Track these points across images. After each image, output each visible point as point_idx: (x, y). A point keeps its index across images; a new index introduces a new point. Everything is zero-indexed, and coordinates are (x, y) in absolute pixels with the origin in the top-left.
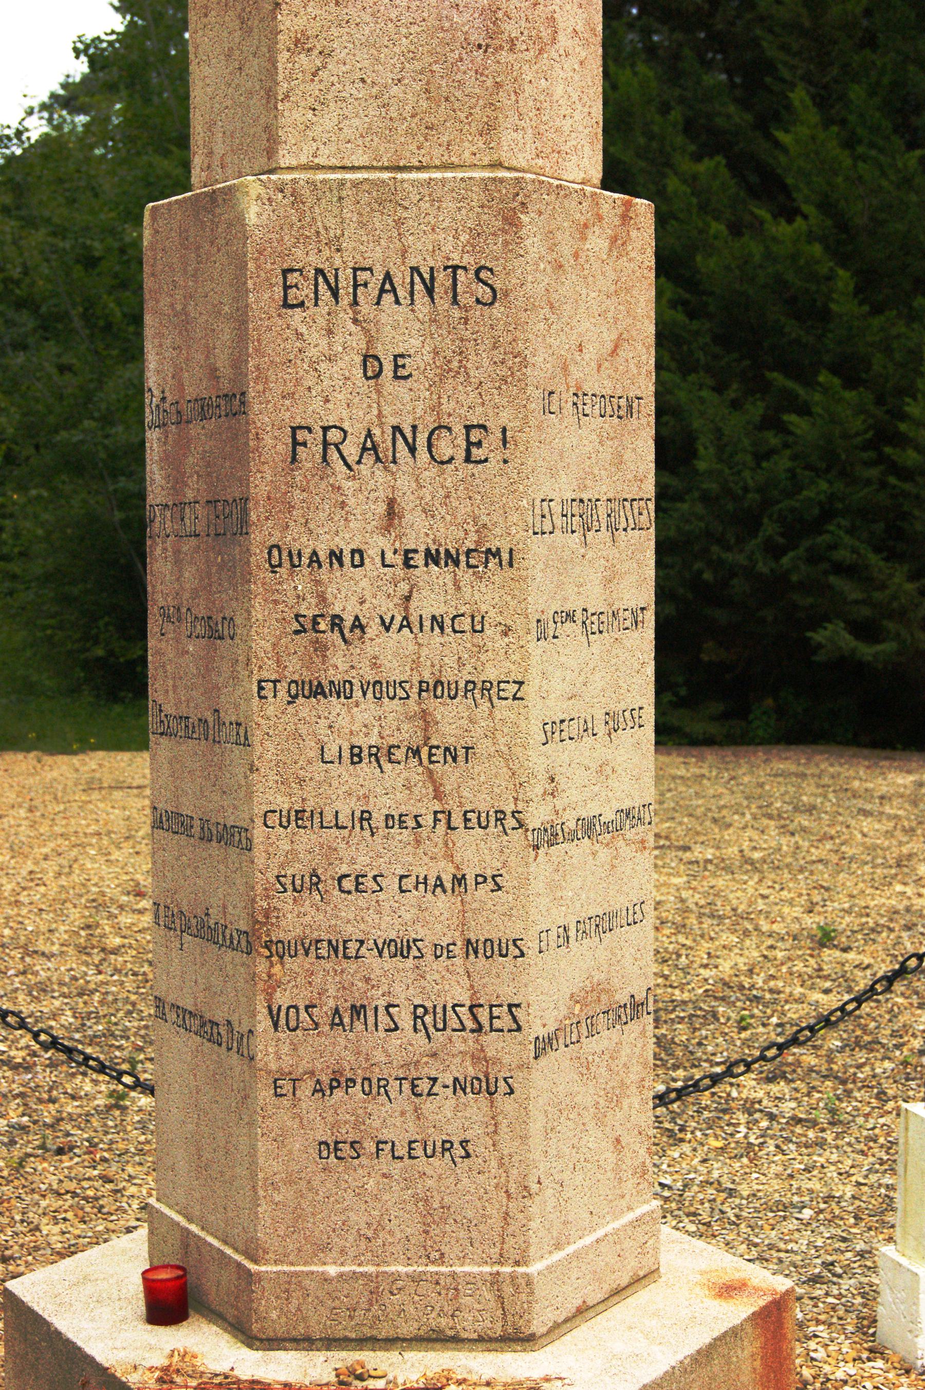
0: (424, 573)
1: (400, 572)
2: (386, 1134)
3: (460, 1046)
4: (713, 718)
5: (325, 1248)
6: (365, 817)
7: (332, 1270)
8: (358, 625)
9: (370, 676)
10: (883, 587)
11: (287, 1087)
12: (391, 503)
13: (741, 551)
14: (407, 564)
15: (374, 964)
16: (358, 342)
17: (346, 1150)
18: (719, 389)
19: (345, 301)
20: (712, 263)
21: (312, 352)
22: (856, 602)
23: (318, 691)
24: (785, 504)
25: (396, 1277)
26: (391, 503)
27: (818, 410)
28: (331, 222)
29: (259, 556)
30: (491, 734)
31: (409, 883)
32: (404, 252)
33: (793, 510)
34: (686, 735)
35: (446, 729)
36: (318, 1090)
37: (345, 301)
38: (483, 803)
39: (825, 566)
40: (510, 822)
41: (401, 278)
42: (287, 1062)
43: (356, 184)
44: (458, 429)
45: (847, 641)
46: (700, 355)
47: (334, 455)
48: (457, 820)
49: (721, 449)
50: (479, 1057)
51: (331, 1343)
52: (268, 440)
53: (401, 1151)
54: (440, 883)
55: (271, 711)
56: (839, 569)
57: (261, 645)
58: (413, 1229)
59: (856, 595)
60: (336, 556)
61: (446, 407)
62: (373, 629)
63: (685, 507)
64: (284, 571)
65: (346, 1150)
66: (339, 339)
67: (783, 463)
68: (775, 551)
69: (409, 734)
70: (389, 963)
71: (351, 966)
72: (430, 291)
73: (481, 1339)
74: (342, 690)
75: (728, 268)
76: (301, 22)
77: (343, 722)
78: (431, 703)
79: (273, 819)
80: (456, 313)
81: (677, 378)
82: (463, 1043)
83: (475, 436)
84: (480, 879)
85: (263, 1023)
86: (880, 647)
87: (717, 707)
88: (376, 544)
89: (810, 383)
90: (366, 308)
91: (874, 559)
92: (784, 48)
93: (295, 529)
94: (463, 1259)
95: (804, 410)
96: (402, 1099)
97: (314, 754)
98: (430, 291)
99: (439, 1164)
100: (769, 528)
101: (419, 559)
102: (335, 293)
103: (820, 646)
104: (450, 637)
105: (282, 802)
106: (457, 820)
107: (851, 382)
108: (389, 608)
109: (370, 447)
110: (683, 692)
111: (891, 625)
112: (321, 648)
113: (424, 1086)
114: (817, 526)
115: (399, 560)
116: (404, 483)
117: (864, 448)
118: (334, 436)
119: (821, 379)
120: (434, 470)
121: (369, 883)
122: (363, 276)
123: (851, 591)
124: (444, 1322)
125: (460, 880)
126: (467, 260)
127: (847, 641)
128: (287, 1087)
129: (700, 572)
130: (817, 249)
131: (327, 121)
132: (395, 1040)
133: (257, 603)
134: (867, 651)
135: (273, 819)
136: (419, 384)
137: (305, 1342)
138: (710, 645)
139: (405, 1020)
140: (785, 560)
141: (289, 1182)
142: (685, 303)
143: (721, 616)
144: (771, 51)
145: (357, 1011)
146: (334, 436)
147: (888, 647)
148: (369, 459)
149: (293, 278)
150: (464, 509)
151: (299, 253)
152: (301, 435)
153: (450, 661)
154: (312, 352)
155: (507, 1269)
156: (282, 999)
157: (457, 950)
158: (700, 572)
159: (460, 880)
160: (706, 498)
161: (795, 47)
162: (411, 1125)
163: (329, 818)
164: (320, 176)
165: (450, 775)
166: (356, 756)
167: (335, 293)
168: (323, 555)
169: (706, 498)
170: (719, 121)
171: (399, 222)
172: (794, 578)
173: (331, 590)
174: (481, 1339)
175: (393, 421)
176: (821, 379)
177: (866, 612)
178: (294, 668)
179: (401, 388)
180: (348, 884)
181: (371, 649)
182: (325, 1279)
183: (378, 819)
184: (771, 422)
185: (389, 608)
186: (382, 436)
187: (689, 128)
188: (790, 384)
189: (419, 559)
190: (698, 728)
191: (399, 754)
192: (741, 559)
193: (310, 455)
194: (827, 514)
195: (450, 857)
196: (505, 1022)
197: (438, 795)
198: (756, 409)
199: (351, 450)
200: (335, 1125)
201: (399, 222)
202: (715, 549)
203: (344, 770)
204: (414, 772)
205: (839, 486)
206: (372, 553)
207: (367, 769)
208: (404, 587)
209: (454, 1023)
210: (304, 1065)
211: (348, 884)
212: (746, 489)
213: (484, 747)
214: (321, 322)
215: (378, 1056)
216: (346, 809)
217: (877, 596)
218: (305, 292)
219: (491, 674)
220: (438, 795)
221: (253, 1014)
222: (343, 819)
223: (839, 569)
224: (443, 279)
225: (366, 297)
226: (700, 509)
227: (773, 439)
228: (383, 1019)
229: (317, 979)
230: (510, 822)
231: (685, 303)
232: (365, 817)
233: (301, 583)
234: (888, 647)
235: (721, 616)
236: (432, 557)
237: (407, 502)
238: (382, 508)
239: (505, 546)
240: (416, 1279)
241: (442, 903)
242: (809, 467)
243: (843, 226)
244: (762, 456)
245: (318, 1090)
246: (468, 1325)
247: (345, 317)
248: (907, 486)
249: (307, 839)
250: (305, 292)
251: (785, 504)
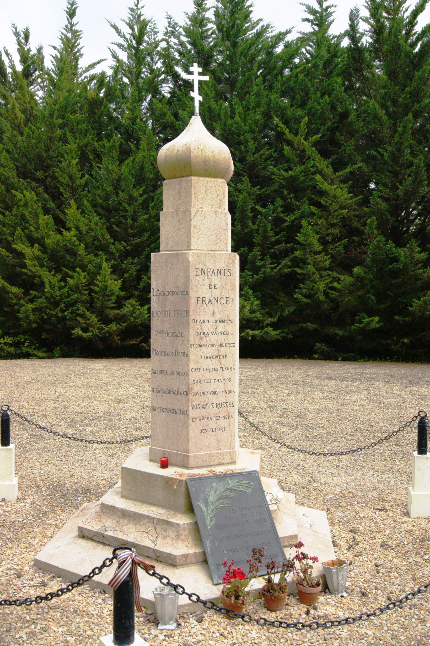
0: (219, 324)
1: (215, 324)
2: (211, 427)
3: (224, 410)
4: (44, 352)
5: (201, 449)
6: (209, 369)
7: (202, 453)
8: (208, 334)
9: (210, 343)
10: (89, 319)
11: (195, 420)
12: (214, 311)
13: (54, 311)
14: (216, 323)
15: (210, 396)
16: (208, 282)
17: (205, 431)
18: (50, 271)
19: (206, 274)
20: (50, 241)
21: (200, 284)
22: (83, 323)
23: (201, 346)
24: (66, 300)
25: (214, 453)
26: (214, 311)
27: (75, 277)
28: (204, 260)
29: (191, 321)
30: (229, 353)
31: (216, 381)
32: (216, 266)
33: (68, 301)
34: (38, 356)
35: (222, 352)
36: (200, 420)
37: (206, 274)
38: (228, 366)
39: (75, 315)
40: (233, 369)
41: (216, 271)
42: (195, 415)
43: (208, 254)
44: (225, 298)
45: (80, 333)
46: (45, 263)
47: (204, 302)
48: (224, 369)
49: (50, 286)
50: (227, 412)
51: (208, 466)
52: (193, 300)
53: (214, 430)
54: (221, 381)
55: (193, 350)
56: (78, 315)
57: (191, 338)
58: (216, 444)
59: (83, 322)
60: (204, 321)
61: (223, 294)
62: (210, 334)
63: (41, 300)
64: (195, 324)
65: (205, 431)
66: (205, 281)
67: (66, 290)
68: (62, 311)
69: (216, 353)
70: (212, 396)
71: (206, 396)
72: (220, 273)
73: (227, 463)
74: (205, 346)
75: (53, 242)
76: (195, 223)
77: (205, 352)
78: (220, 348)
79: (193, 370)
80: (225, 277)
81: (40, 268)
82: (224, 409)
83: (227, 299)
84: (228, 379)
85: (191, 408)
86: (88, 334)
87: (45, 349)
88: (211, 319)
89: (75, 271)
90: (210, 276)
91: (88, 313)
92: (64, 189)
93: (197, 316)
94: (224, 449)
95: (71, 277)
96: (214, 420)
97: (200, 357)
98: (220, 273)
99: (220, 432)
100: (62, 305)
101: (218, 321)
102: (204, 273)
103: (74, 334)
104: (223, 336)
105: (194, 367)
106: (224, 369)
107: (84, 271)
108: (213, 330)
109: (210, 301)
110: (37, 345)
111: (91, 329)
112: (201, 338)
113: (218, 418)
114: (73, 305)
115: (215, 322)
116: (216, 308)
117: (85, 286)
118: (204, 299)
119: (77, 270)
120: (221, 305)
121: (209, 381)
122: (209, 270)
123: (81, 321)
124: (221, 461)
125: (224, 380)
126: (226, 268)
127: (80, 333)
128: (195, 420)
129: (43, 316)
130: (75, 239)
131: (199, 241)
132: (213, 410)
133: (190, 330)
134: (85, 335)
135: (193, 370)
136: (218, 290)
137: (203, 467)
138: (44, 334)
139: (215, 405)
140: (66, 313)
141: (195, 438)
142: (40, 250)
143: (48, 327)
144: (62, 190)
145: (207, 405)
146: (204, 299)
147: (90, 334)
148: (210, 303)
149: (197, 270)
150: (225, 313)
151: (198, 266)
152: (199, 299)
153: (223, 340)
154: (200, 284)
155: (232, 450)
156: (194, 404)
157: (224, 393)
158: (43, 316)
159: (224, 380)
160: (46, 298)
161: (67, 190)
162: (216, 425)
163: (202, 369)
164: (204, 252)
165: (222, 360)
166: (207, 358)
167: (204, 273)
168: (202, 321)
169: (46, 298)
170: (48, 206)
171: (215, 261)
172: (68, 317)
173: (203, 327)
174: (227, 463)
175: (214, 297)
176: (77, 270)
177: (85, 325)
178: (197, 342)
179: (215, 290)
180: (205, 381)
181: (210, 338)
182: (201, 455)
183: (211, 369)
184: (63, 279)
185: (213, 330)
186: (212, 300)
187: (43, 208)
188: (67, 270)
189: (218, 321)
190: (41, 354)
191: (214, 357)
192: (54, 313)
193: (200, 303)
194: (76, 302)
195: (222, 375)
196: (231, 405)
197: (221, 364)
198: (60, 276)
199: (207, 302)
200: (203, 426)
201: (215, 261)
202: (48, 310)
203: (205, 360)
204: (216, 360)
205: (79, 295)
206: (210, 321)
207: (209, 360)
208: (215, 327)
209: (223, 406)
210: (197, 416)
211: (205, 381)
212: (56, 296)
213: (228, 355)
214: (202, 278)
215: (211, 413)
216: (205, 367)
217: (88, 322)
218: (199, 273)
219: (230, 342)
220: (221, 364)
221: (189, 407)
222: (205, 370)
223: (78, 315)
224: (222, 271)
225: (210, 274)
226: (45, 301)
227: (63, 284)
228: (211, 406)
229: (200, 399)
230: (233, 369)
231: (40, 250)
232: (209, 369)
233: (198, 326)
234: (90, 334)
235: (48, 327)
236: (220, 321)
237: (216, 311)
238: (212, 312)
239: (232, 319)
240: (217, 453)
241: (221, 384)
242: (72, 291)
243: (80, 233)
244: (60, 288)
245: (200, 420)
246: (225, 461)
247: (206, 278)
248: (96, 296)
249: (199, 373)
250: (199, 273)
251: (66, 300)
